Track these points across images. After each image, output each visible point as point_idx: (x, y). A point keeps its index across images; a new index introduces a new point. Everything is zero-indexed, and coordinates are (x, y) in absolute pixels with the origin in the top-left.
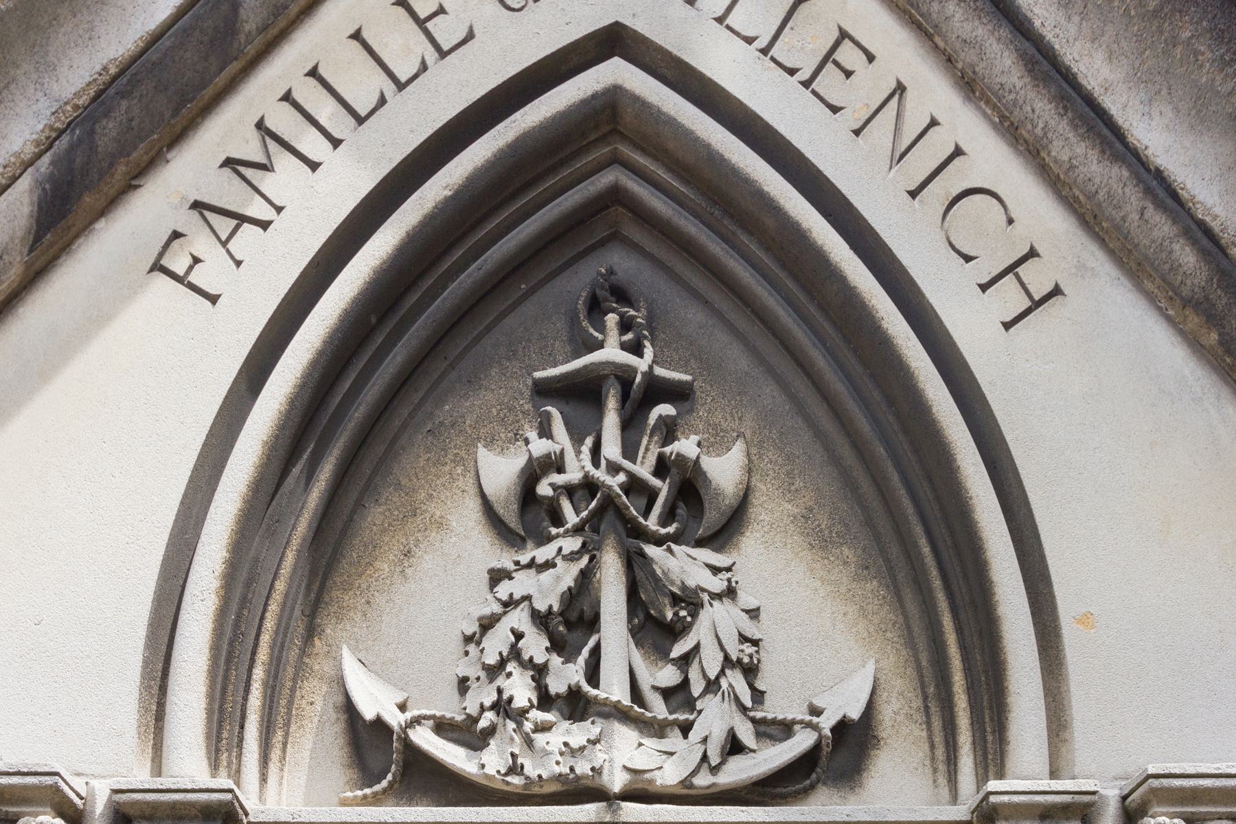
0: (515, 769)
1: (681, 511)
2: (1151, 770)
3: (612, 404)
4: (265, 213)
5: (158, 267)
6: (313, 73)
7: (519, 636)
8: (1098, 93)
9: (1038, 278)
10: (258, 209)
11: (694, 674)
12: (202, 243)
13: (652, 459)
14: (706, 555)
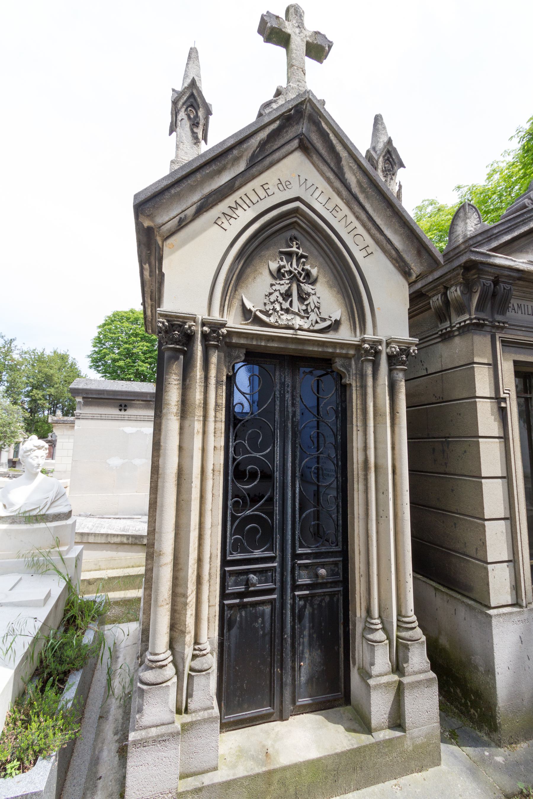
0: (277, 322)
1: (306, 278)
2: (392, 337)
3: (295, 258)
4: (236, 217)
5: (215, 223)
6: (246, 194)
7: (278, 297)
8: (379, 225)
9: (369, 250)
10: (234, 216)
11: (309, 308)
12: (224, 220)
13: (301, 268)
14: (310, 286)
